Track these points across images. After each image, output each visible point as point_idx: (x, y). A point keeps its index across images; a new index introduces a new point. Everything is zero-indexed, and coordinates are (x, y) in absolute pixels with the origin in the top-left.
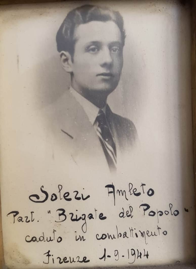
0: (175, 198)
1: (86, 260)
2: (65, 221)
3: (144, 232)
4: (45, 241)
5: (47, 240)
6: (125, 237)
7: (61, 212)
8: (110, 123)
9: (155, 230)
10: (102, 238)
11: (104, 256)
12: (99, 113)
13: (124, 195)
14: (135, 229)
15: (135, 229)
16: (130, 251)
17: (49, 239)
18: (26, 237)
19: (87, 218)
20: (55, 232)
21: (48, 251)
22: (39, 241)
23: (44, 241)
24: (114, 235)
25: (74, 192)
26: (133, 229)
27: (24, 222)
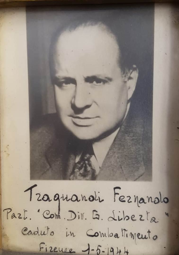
0: (174, 220)
1: (72, 251)
3: (104, 236)
4: (39, 235)
5: (41, 234)
11: (89, 249)
13: (136, 202)
17: (42, 233)
20: (49, 229)
22: (43, 235)
23: (39, 235)
24: (105, 233)
25: (144, 220)
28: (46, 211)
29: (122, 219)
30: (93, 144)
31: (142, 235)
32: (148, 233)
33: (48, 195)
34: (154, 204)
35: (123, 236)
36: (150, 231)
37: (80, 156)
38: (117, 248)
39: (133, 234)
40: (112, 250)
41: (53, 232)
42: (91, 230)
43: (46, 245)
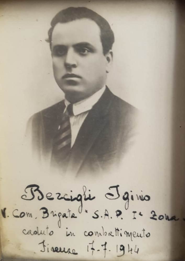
6: (29, 234)
7: (45, 210)
8: (60, 128)
9: (140, 232)
10: (89, 235)
16: (119, 247)
18: (14, 210)
19: (61, 217)
21: (42, 241)
25: (56, 194)
26: (119, 229)
28: (108, 199)
30: (123, 153)
31: (138, 234)
32: (69, 212)
34: (141, 201)
35: (116, 235)
36: (145, 229)
38: (102, 227)
39: (28, 213)
40: (122, 248)
42: (17, 210)
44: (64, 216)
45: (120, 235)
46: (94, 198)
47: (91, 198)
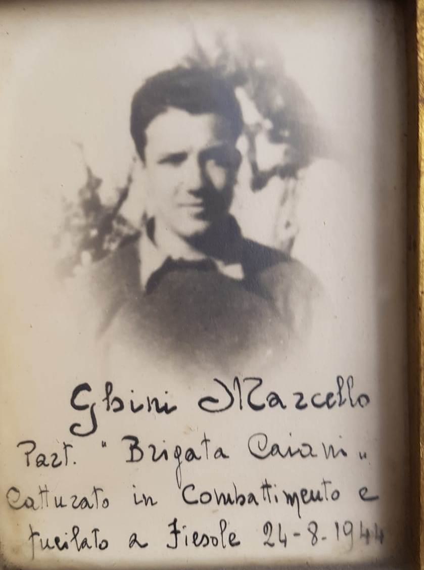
2: (248, 448)
6: (252, 501)
8: (224, 278)
12: (87, 214)
14: (275, 486)
15: (275, 486)
18: (18, 499)
19: (182, 457)
21: (172, 521)
22: (22, 506)
27: (92, 548)
29: (141, 407)
31: (312, 492)
33: (70, 405)
35: (265, 499)
37: (220, 264)
38: (186, 544)
41: (106, 500)
43: (296, 535)
44: (191, 455)
45: (273, 499)
46: (174, 408)
47: (169, 407)
